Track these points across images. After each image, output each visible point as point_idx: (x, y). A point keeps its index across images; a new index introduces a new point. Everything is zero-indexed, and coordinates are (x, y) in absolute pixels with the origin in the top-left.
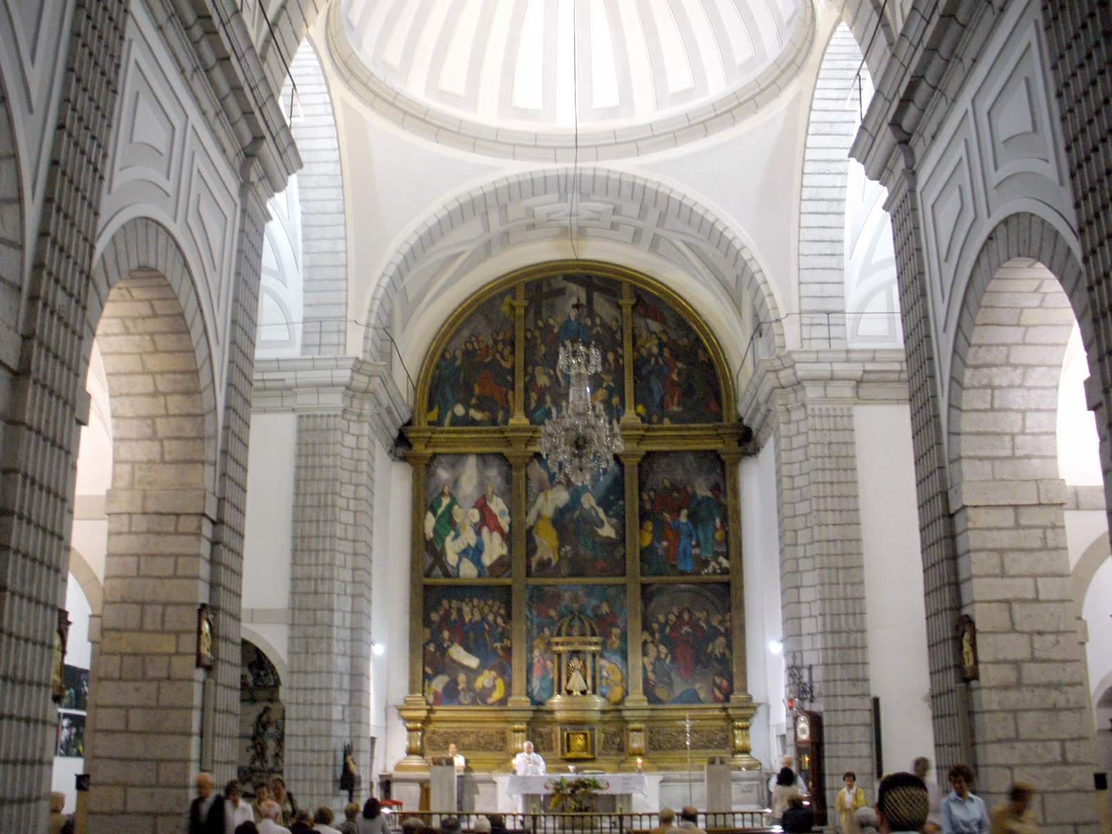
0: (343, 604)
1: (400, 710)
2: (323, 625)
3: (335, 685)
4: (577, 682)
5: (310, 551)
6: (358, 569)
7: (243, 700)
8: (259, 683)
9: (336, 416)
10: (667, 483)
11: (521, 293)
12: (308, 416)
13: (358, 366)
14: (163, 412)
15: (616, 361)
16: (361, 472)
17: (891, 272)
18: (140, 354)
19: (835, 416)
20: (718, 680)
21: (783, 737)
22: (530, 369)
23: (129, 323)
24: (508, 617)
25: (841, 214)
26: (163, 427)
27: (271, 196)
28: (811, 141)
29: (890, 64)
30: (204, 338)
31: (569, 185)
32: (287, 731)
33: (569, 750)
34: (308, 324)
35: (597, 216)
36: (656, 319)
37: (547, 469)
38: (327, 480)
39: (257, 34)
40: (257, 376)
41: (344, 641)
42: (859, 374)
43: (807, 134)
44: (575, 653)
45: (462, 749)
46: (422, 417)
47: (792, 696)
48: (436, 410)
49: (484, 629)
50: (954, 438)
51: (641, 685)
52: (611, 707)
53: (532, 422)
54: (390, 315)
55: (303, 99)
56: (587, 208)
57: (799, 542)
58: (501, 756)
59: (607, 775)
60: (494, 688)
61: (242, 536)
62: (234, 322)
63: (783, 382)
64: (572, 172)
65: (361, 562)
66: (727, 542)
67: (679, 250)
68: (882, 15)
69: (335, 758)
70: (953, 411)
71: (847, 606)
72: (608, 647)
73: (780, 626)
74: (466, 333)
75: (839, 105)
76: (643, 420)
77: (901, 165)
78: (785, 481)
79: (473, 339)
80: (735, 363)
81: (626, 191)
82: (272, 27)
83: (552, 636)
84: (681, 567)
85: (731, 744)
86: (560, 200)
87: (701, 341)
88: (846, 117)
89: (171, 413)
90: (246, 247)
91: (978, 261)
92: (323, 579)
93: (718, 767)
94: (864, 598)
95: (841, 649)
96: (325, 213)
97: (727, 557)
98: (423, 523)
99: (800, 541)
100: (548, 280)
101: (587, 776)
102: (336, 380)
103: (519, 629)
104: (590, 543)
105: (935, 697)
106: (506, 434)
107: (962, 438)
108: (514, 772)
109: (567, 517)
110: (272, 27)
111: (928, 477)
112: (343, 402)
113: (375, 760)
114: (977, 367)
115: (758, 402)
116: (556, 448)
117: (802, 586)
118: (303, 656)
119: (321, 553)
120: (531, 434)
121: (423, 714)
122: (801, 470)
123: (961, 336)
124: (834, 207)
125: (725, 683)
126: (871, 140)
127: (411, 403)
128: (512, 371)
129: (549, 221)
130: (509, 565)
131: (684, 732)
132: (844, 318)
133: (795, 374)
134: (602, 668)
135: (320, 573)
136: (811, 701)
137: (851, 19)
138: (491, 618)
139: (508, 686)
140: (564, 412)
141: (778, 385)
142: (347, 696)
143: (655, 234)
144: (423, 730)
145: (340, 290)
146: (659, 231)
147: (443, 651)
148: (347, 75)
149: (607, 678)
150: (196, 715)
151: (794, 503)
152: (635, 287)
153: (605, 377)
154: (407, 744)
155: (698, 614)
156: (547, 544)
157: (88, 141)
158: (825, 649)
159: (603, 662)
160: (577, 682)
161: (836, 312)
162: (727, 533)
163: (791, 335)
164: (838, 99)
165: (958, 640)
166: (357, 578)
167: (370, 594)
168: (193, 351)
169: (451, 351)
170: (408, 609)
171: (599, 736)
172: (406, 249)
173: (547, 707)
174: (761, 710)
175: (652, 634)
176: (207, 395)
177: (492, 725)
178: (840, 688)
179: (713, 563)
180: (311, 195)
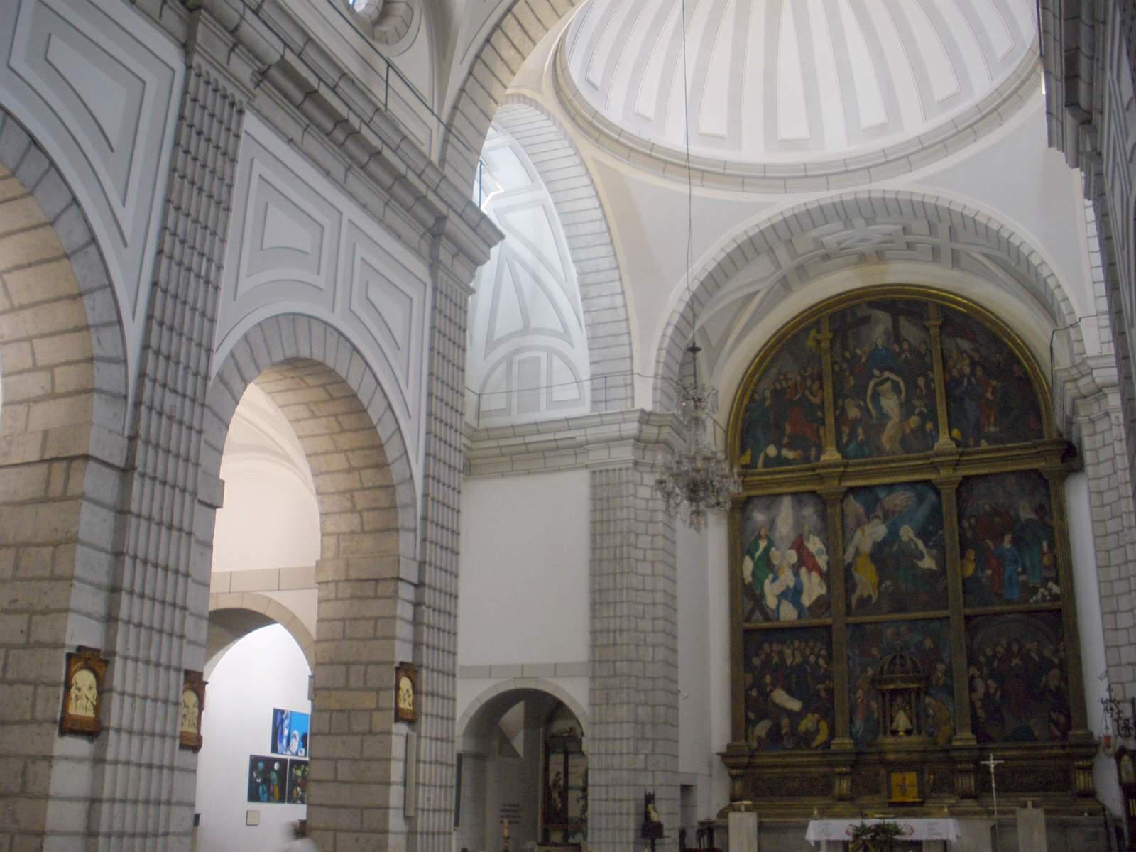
9: (627, 469)
12: (601, 472)
13: (646, 418)
15: (927, 385)
16: (657, 522)
18: (330, 434)
20: (1054, 716)
22: (840, 403)
23: (313, 408)
26: (361, 502)
31: (842, 212)
38: (621, 532)
48: (749, 452)
53: (843, 457)
60: (818, 731)
63: (1084, 392)
66: (1055, 565)
67: (978, 261)
74: (774, 371)
76: (958, 444)
79: (781, 377)
86: (846, 227)
89: (366, 486)
92: (621, 631)
96: (598, 271)
97: (1057, 582)
99: (1114, 561)
102: (625, 433)
106: (818, 472)
118: (604, 707)
119: (618, 605)
120: (842, 469)
125: (1062, 719)
128: (821, 407)
135: (618, 625)
138: (812, 659)
143: (952, 250)
145: (624, 345)
147: (765, 695)
148: (596, 135)
152: (943, 307)
155: (1028, 645)
156: (866, 579)
157: (196, 258)
160: (902, 721)
162: (1055, 558)
169: (760, 392)
175: (980, 669)
179: (1042, 590)
180: (582, 255)
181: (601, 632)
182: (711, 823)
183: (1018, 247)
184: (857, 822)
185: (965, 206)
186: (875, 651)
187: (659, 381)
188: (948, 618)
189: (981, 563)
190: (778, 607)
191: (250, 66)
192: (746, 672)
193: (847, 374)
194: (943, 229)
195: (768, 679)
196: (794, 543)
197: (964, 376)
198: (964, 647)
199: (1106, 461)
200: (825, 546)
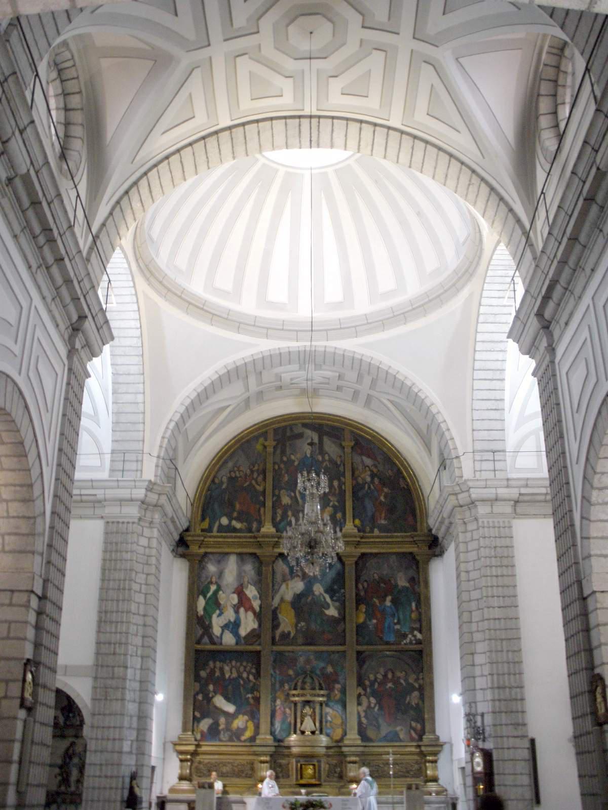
0: (135, 662)
1: (175, 744)
2: (118, 678)
3: (126, 724)
4: (308, 724)
5: (111, 622)
6: (146, 637)
7: (54, 736)
8: (68, 723)
9: (133, 523)
10: (376, 576)
11: (271, 436)
12: (113, 522)
13: (151, 487)
14: (5, 514)
15: (340, 487)
17: (538, 422)
19: (499, 527)
20: (414, 724)
21: (463, 769)
24: (258, 675)
25: (503, 380)
27: (90, 360)
28: (481, 328)
29: (535, 271)
30: (37, 460)
31: (307, 358)
32: (87, 761)
33: (301, 778)
34: (114, 455)
35: (327, 381)
36: (369, 456)
37: (288, 564)
39: (84, 243)
40: (75, 492)
41: (134, 691)
42: (516, 496)
43: (478, 322)
44: (307, 703)
45: (221, 776)
46: (198, 525)
47: (469, 736)
48: (207, 520)
49: (239, 683)
50: (585, 541)
51: (356, 727)
52: (334, 744)
54: (175, 450)
55: (116, 291)
56: (319, 375)
57: (473, 620)
58: (250, 782)
59: (330, 797)
60: (245, 729)
61: (60, 609)
62: (60, 450)
63: (461, 503)
64: (308, 349)
65: (149, 631)
66: (420, 620)
68: (528, 238)
69: (123, 782)
70: (585, 522)
71: (509, 668)
72: (332, 698)
73: (460, 683)
74: (230, 464)
75: (500, 302)
76: (359, 531)
77: (544, 343)
78: (463, 575)
79: (236, 469)
80: (426, 489)
81: (348, 363)
82: (95, 238)
83: (290, 689)
84: (386, 638)
85: (424, 774)
86: (300, 369)
87: (402, 473)
88: (506, 310)
89: (11, 515)
90: (71, 395)
91: (599, 412)
92: (120, 644)
93: (413, 792)
94: (522, 662)
95: (505, 700)
96: (129, 374)
97: (420, 632)
98: (196, 604)
100: (291, 427)
101: (315, 798)
102: (134, 496)
103: (265, 683)
104: (319, 622)
105: (577, 737)
106: (258, 539)
107: (592, 541)
108: (260, 794)
109: (303, 600)
110: (95, 238)
111: (567, 570)
112: (139, 512)
113: (154, 785)
114: (601, 489)
115: (443, 517)
116: (295, 547)
117: (476, 653)
121: (191, 748)
122: (474, 567)
123: (589, 467)
124: (497, 375)
126: (523, 326)
127: (189, 515)
128: (264, 493)
129: (292, 384)
130: (259, 636)
131: (388, 764)
132: (505, 455)
133: (470, 496)
134: (327, 714)
136: (484, 741)
137: (507, 240)
138: (245, 675)
139: (257, 728)
140: (301, 521)
141: (458, 505)
142: (134, 733)
144: (191, 761)
146: (372, 392)
147: (209, 700)
148: (148, 275)
149: (331, 722)
150: (17, 747)
151: (469, 591)
153: (332, 498)
154: (179, 771)
156: (287, 622)
158: (493, 700)
159: (328, 710)
160: (308, 724)
161: (499, 451)
162: (420, 614)
163: (467, 468)
164: (499, 298)
165: (592, 692)
166: (146, 644)
167: (155, 656)
168: (29, 470)
170: (183, 667)
171: (324, 767)
172: (188, 401)
173: (286, 744)
174: (446, 747)
175: (365, 689)
176: (39, 503)
177: (244, 757)
178: (505, 731)
179: (410, 636)
180: (119, 360)
181: (104, 643)
183: (423, 400)
185: (390, 367)
187: (161, 461)
189: (370, 615)
190: (222, 634)
191: (6, 172)
192: (195, 681)
194: (367, 380)
196: (237, 589)
199: (473, 550)
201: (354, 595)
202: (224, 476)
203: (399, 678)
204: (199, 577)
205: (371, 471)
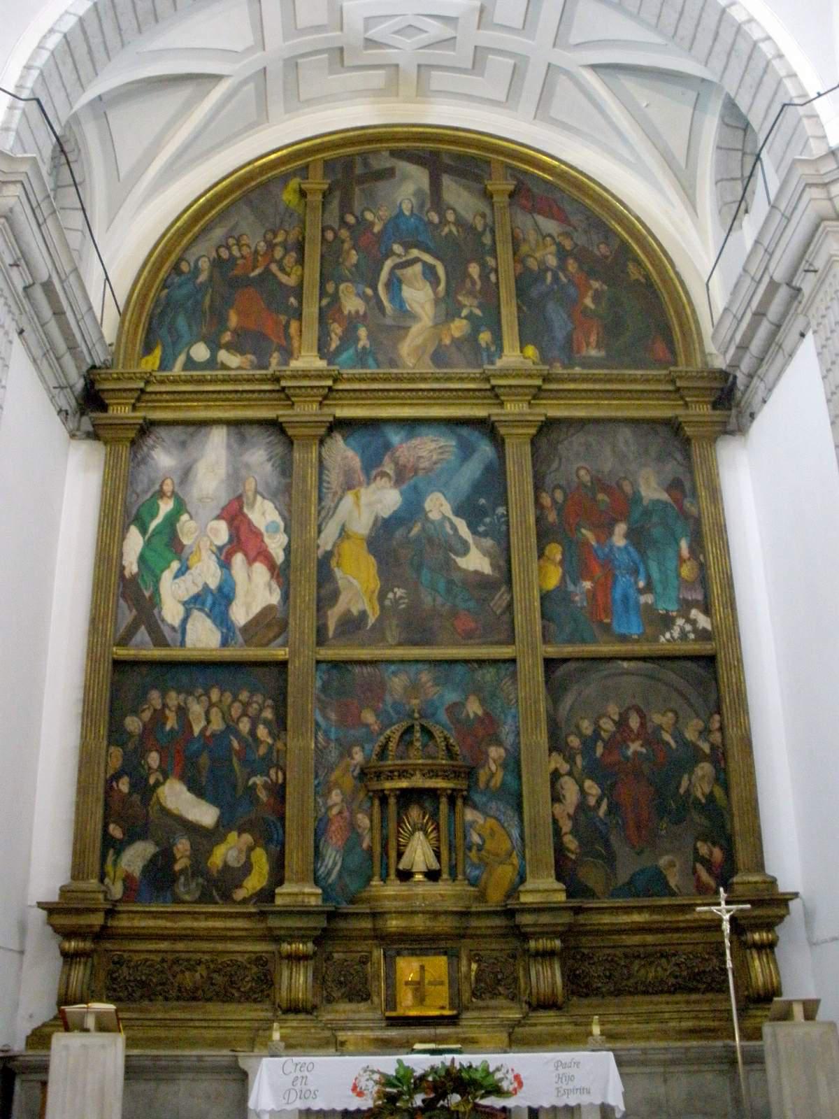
10: (586, 478)
15: (484, 276)
20: (703, 849)
22: (330, 288)
24: (280, 724)
36: (550, 215)
48: (158, 352)
60: (247, 868)
66: (703, 580)
79: (231, 241)
84: (619, 628)
97: (707, 610)
104: (442, 585)
106: (283, 383)
109: (399, 533)
128: (298, 291)
130: (284, 626)
138: (244, 726)
147: (145, 790)
155: (657, 719)
160: (419, 853)
162: (703, 567)
170: (78, 709)
172: (70, 23)
175: (570, 759)
179: (680, 622)
182: (13, 1058)
184: (388, 1064)
186: (369, 717)
188: (513, 661)
189: (576, 565)
193: (346, 246)
195: (154, 759)
197: (547, 269)
198: (543, 716)
200: (284, 518)
201: (532, 520)
202: (202, 257)
203: (660, 727)
204: (130, 481)
205: (559, 245)
